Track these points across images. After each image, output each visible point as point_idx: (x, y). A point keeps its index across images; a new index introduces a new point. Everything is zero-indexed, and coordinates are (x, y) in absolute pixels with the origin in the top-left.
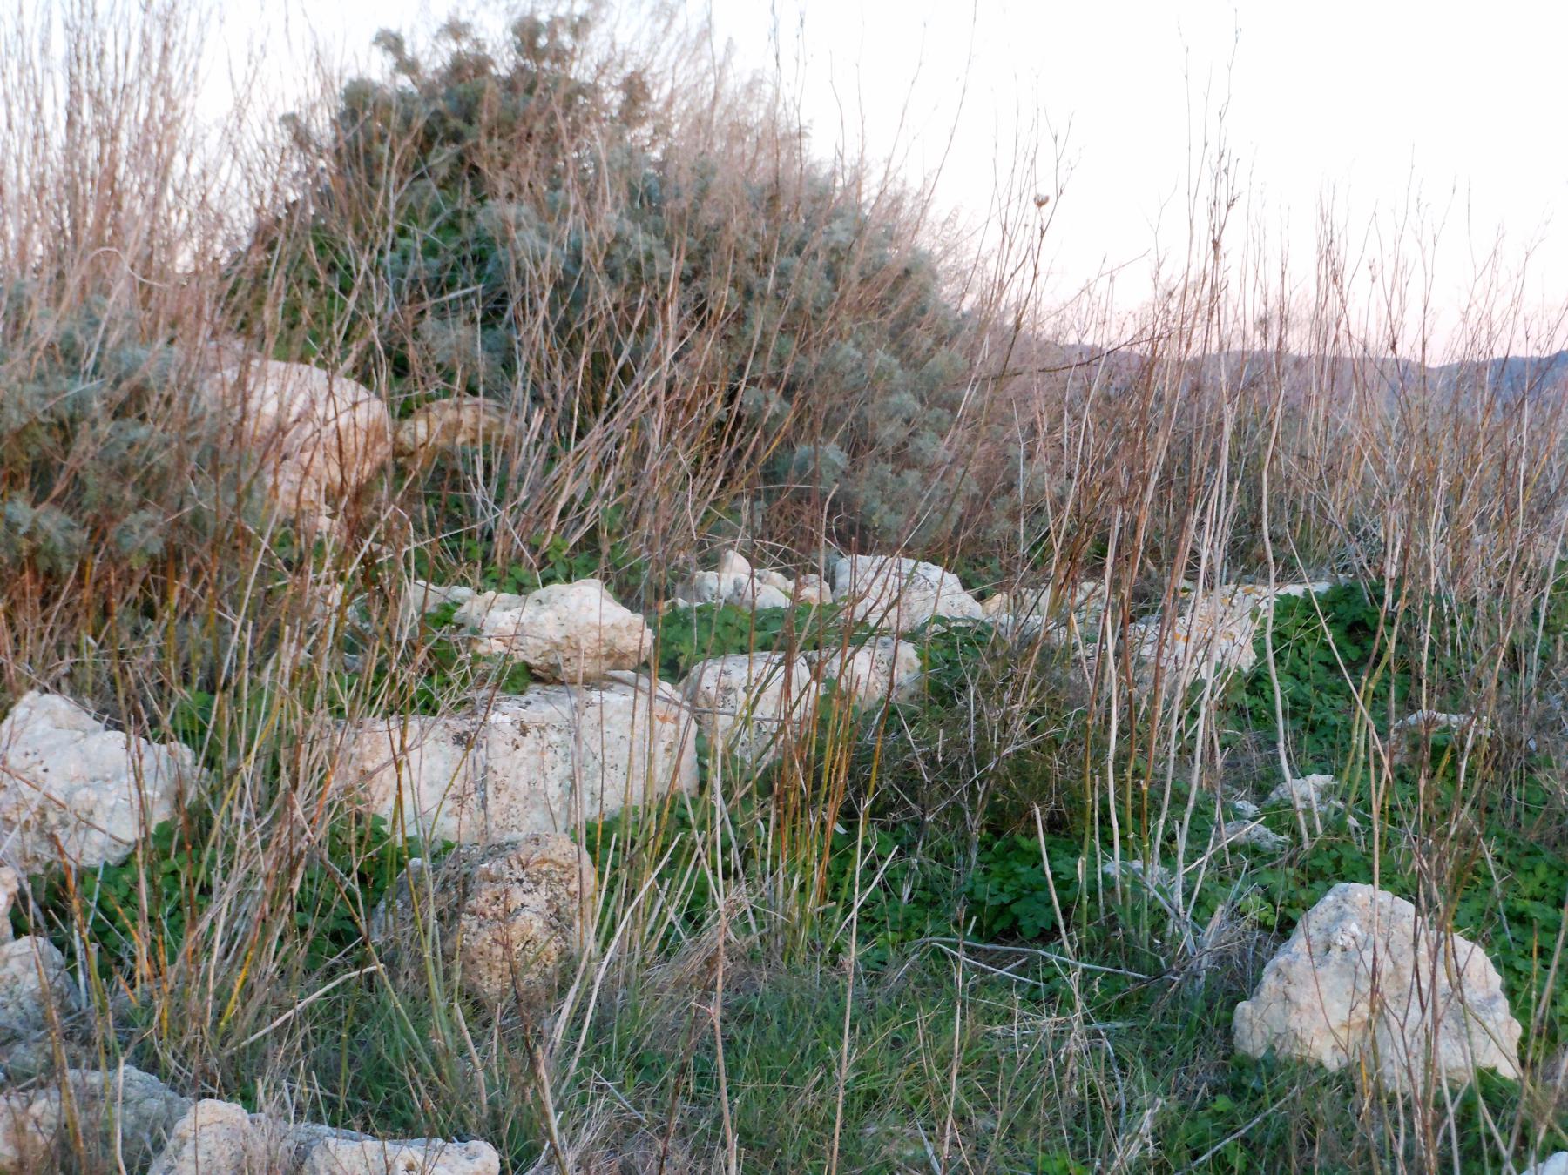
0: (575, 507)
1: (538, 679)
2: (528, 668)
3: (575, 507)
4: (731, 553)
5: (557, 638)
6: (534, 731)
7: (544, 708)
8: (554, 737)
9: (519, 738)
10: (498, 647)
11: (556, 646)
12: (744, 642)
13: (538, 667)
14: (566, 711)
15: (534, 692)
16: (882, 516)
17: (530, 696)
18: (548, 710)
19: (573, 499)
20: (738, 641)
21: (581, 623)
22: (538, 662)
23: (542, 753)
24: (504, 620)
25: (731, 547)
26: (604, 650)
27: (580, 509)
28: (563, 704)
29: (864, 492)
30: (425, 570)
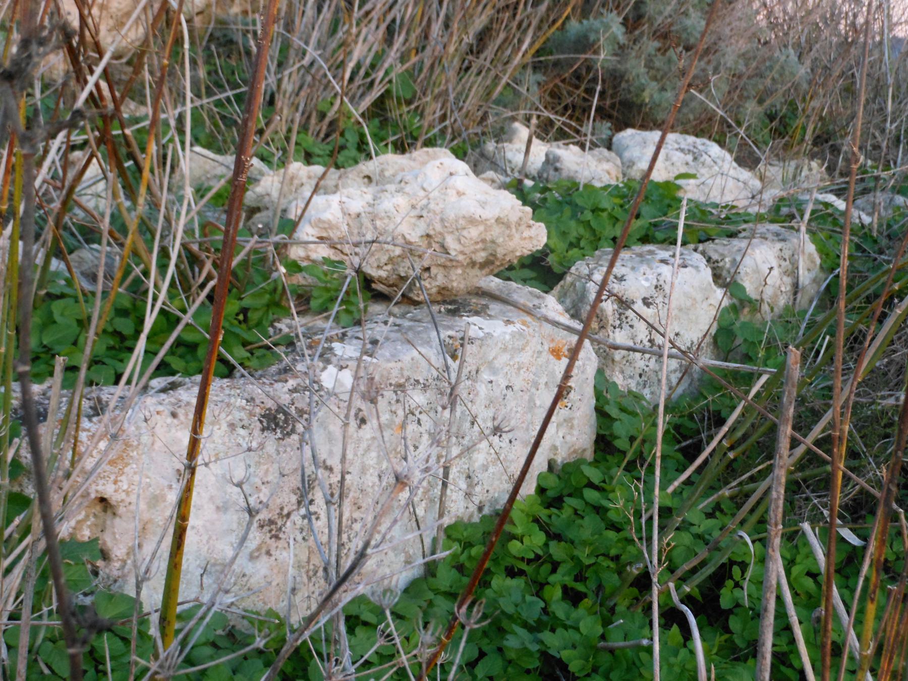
0: (362, 72)
1: (381, 297)
2: (367, 282)
3: (362, 72)
4: (517, 125)
5: (414, 236)
6: (389, 394)
7: (408, 354)
8: (418, 398)
9: (365, 406)
10: (322, 252)
11: (410, 250)
12: (618, 232)
13: (380, 280)
14: (433, 353)
15: (380, 320)
16: (650, 93)
17: (378, 330)
18: (409, 355)
19: (358, 66)
20: (610, 231)
21: (451, 215)
22: (383, 274)
23: (403, 426)
24: (338, 210)
25: (514, 119)
26: (481, 257)
27: (367, 74)
28: (428, 343)
29: (636, 68)
30: (202, 137)
